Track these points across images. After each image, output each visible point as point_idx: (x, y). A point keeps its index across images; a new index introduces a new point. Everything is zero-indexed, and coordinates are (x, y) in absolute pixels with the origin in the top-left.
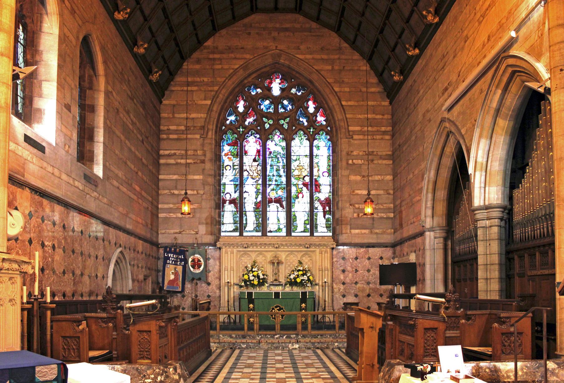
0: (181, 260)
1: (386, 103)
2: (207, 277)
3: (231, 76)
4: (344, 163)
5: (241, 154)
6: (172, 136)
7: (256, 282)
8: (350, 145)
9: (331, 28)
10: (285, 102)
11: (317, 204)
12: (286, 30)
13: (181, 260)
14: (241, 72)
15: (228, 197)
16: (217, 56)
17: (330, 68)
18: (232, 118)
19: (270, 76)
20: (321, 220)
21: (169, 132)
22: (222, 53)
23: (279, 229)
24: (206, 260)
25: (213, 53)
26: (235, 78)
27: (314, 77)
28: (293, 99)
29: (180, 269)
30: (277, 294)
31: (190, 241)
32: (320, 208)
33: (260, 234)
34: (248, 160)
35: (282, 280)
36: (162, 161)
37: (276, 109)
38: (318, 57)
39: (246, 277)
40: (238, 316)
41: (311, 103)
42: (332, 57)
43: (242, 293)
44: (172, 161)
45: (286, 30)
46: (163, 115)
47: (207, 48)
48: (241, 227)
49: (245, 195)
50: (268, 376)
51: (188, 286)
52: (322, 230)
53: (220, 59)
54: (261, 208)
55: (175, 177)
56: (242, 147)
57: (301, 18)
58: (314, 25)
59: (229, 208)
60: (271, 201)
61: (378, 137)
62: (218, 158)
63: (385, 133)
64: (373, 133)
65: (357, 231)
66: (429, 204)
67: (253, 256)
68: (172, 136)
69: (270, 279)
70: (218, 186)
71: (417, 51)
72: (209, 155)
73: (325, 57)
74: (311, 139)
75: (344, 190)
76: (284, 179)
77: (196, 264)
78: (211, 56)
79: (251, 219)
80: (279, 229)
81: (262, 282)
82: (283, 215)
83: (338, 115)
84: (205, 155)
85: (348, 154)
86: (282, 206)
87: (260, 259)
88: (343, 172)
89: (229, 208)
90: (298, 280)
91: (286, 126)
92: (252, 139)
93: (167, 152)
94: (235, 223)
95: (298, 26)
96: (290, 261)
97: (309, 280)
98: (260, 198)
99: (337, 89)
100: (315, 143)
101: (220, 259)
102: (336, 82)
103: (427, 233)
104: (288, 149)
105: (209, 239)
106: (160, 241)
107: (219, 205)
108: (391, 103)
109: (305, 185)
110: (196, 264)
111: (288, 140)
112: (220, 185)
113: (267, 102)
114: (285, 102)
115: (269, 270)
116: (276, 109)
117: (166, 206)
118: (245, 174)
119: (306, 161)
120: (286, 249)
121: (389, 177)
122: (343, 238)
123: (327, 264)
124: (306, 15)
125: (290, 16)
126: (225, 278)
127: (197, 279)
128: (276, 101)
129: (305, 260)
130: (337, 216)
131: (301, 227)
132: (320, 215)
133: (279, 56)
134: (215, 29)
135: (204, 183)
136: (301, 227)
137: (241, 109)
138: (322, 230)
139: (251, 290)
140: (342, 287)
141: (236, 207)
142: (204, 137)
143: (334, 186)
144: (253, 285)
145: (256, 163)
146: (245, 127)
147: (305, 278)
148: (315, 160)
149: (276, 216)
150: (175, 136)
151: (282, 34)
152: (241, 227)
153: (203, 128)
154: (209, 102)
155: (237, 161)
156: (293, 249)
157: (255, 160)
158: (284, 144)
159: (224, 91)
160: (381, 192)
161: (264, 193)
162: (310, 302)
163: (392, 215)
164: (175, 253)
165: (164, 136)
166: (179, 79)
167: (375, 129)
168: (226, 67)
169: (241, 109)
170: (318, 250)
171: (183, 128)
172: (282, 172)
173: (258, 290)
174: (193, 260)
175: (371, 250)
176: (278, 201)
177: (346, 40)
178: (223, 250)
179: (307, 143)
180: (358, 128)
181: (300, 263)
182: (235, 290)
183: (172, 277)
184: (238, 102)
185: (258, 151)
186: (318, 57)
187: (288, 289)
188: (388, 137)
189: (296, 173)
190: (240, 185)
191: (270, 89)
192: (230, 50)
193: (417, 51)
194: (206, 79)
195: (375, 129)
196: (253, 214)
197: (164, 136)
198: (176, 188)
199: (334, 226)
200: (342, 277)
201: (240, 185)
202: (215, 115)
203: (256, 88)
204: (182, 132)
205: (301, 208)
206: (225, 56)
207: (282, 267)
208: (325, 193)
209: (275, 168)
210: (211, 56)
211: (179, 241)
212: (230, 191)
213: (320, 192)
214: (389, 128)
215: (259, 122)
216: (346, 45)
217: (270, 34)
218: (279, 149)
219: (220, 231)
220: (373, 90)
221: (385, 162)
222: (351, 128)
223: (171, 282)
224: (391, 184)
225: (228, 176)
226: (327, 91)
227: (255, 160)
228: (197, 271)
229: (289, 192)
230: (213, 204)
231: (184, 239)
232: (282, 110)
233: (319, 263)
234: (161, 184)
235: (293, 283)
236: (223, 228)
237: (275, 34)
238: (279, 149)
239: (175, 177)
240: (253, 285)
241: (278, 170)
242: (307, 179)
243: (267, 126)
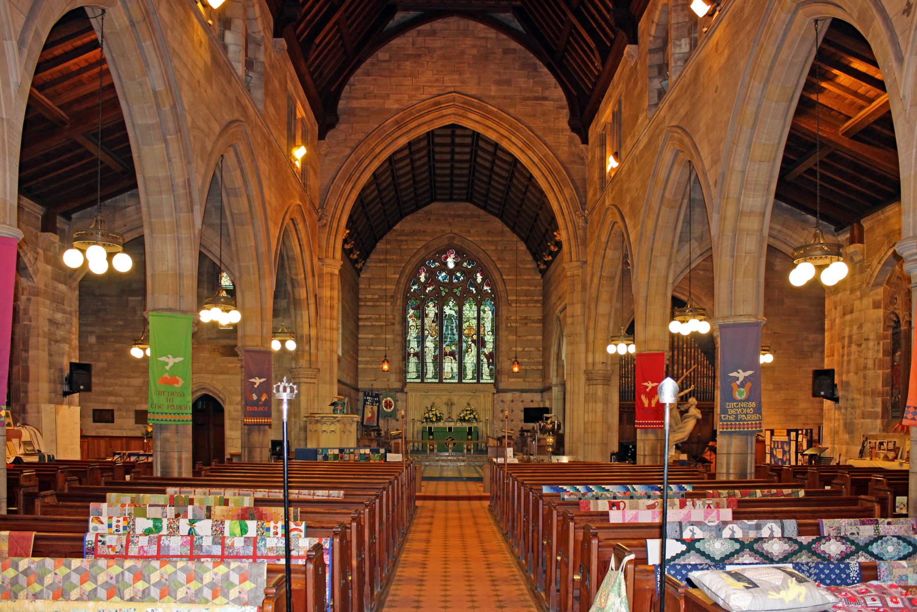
0: (376, 402)
1: (539, 277)
2: (396, 415)
3: (415, 254)
4: (504, 326)
5: (422, 316)
6: (368, 304)
7: (434, 419)
8: (509, 311)
9: (497, 215)
10: (458, 274)
11: (482, 357)
12: (459, 216)
13: (376, 402)
14: (423, 251)
15: (412, 351)
16: (404, 238)
17: (494, 248)
18: (415, 287)
19: (444, 251)
20: (486, 369)
21: (366, 300)
22: (406, 235)
23: (453, 378)
24: (396, 401)
25: (400, 235)
26: (418, 256)
27: (481, 255)
28: (464, 272)
29: (375, 408)
30: (450, 429)
31: (383, 387)
32: (485, 360)
33: (437, 381)
34: (428, 321)
35: (455, 417)
36: (360, 323)
37: (451, 279)
38: (485, 239)
39: (427, 415)
40: (420, 444)
41: (478, 275)
42: (496, 239)
43: (424, 428)
44: (368, 324)
45: (459, 216)
46: (361, 286)
47: (396, 231)
48: (422, 374)
49: (426, 350)
50: (466, 179)
51: (381, 422)
52: (486, 378)
53: (406, 241)
54: (438, 362)
55: (371, 336)
56: (424, 310)
57: (471, 206)
58: (482, 212)
59: (413, 360)
60: (446, 355)
61: (532, 305)
62: (404, 321)
63: (537, 301)
64: (527, 302)
65: (513, 380)
66: (555, 368)
67: (433, 399)
68: (368, 304)
69: (445, 417)
70: (405, 343)
71: (550, 258)
72: (398, 319)
73: (490, 239)
74: (479, 305)
75: (504, 347)
76: (456, 337)
77: (388, 405)
78: (399, 238)
79: (430, 368)
80: (453, 378)
81: (439, 419)
82: (455, 366)
83: (500, 287)
84: (394, 319)
85: (507, 319)
86: (455, 358)
87: (437, 401)
88: (503, 333)
89: (413, 360)
90: (467, 418)
91: (458, 294)
92: (431, 305)
93: (364, 316)
94: (417, 371)
95: (468, 213)
96: (461, 402)
97: (475, 418)
98: (437, 352)
99: (499, 266)
100: (482, 307)
101: (406, 401)
102: (499, 259)
103: (553, 388)
104: (460, 313)
105: (397, 385)
106: (359, 387)
107: (405, 357)
108: (542, 277)
109: (473, 341)
110: (388, 405)
111: (460, 306)
112: (406, 341)
113: (444, 274)
114: (458, 274)
115: (444, 410)
116: (451, 279)
117: (364, 359)
118: (426, 332)
119: (474, 322)
120: (458, 393)
121: (540, 337)
122: (502, 386)
123: (489, 406)
124: (475, 204)
125: (463, 204)
126: (410, 416)
127: (388, 416)
128: (451, 273)
129: (472, 402)
130: (498, 367)
131: (470, 376)
132: (485, 366)
133: (454, 238)
134: (402, 216)
135: (394, 341)
136: (470, 376)
137: (423, 279)
138: (486, 378)
139: (431, 425)
140: (501, 424)
141: (418, 359)
142: (394, 303)
143: (496, 342)
144: (432, 421)
145: (434, 324)
146: (425, 294)
147: (472, 416)
148: (482, 322)
149: (450, 366)
150: (371, 304)
151: (456, 220)
152: (422, 374)
153: (392, 297)
154: (397, 276)
155: (419, 322)
156: (463, 393)
157: (433, 322)
158: (456, 308)
159: (409, 267)
160: (533, 349)
161: (441, 348)
162: (474, 435)
163: (541, 367)
164: (372, 396)
165: (362, 303)
166: (373, 256)
167: (529, 298)
168: (411, 247)
169: (423, 279)
170: (482, 395)
171: (377, 297)
172: (455, 331)
173: (436, 425)
174: (386, 402)
175: (524, 394)
176: (452, 354)
177: (508, 225)
178: (409, 394)
179: (474, 308)
180: (514, 298)
181: (468, 404)
182: (418, 426)
183: (370, 415)
184: (420, 274)
185: (436, 314)
186: (485, 239)
187: (459, 425)
188: (539, 305)
189: (466, 332)
190: (421, 340)
191: (446, 264)
192: (414, 233)
193: (550, 258)
194: (395, 257)
195: (529, 298)
196: (431, 365)
197: (362, 303)
198: (372, 345)
199: (495, 374)
200: (501, 415)
201: (421, 340)
202: (402, 286)
203: (434, 262)
204: (377, 300)
205: (470, 360)
206: (410, 238)
207: (454, 408)
208: (489, 348)
209: (450, 331)
210: (399, 238)
211: (375, 387)
212: (414, 345)
213: (485, 347)
214: (541, 298)
215: (437, 291)
216: (508, 229)
217: (446, 219)
218: (453, 313)
219: (406, 378)
220: (528, 266)
221: (536, 325)
222: (510, 298)
223: (369, 419)
224: (541, 343)
225: (413, 334)
226: (492, 267)
227: (433, 322)
228: (389, 410)
229: (461, 347)
230: (401, 357)
231: (378, 385)
232: (455, 281)
233: (483, 404)
234: (360, 341)
235: (463, 420)
236: (409, 376)
237: (450, 220)
238: (453, 313)
239: (371, 336)
240: (432, 421)
241: (452, 330)
242: (475, 337)
243: (444, 294)
